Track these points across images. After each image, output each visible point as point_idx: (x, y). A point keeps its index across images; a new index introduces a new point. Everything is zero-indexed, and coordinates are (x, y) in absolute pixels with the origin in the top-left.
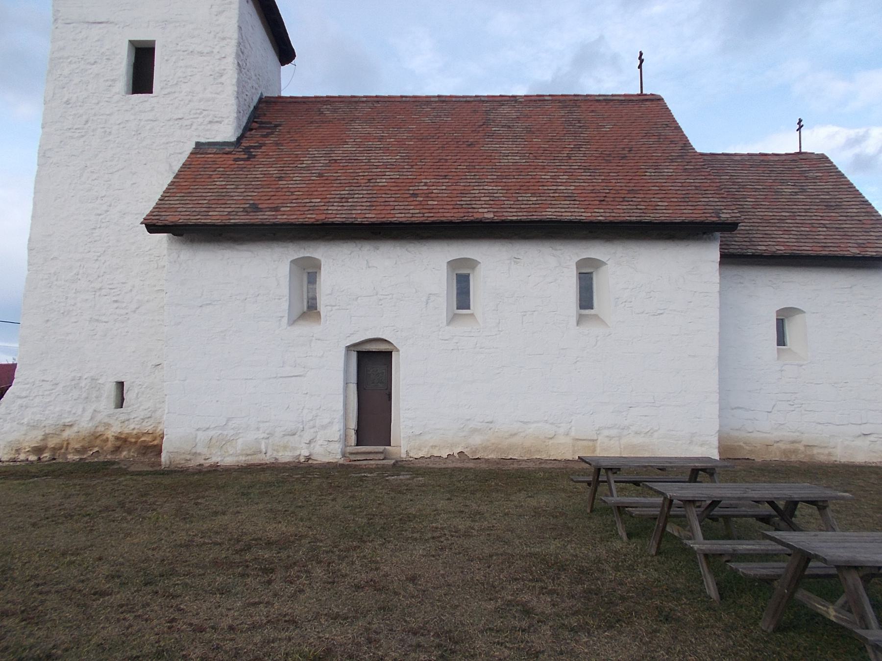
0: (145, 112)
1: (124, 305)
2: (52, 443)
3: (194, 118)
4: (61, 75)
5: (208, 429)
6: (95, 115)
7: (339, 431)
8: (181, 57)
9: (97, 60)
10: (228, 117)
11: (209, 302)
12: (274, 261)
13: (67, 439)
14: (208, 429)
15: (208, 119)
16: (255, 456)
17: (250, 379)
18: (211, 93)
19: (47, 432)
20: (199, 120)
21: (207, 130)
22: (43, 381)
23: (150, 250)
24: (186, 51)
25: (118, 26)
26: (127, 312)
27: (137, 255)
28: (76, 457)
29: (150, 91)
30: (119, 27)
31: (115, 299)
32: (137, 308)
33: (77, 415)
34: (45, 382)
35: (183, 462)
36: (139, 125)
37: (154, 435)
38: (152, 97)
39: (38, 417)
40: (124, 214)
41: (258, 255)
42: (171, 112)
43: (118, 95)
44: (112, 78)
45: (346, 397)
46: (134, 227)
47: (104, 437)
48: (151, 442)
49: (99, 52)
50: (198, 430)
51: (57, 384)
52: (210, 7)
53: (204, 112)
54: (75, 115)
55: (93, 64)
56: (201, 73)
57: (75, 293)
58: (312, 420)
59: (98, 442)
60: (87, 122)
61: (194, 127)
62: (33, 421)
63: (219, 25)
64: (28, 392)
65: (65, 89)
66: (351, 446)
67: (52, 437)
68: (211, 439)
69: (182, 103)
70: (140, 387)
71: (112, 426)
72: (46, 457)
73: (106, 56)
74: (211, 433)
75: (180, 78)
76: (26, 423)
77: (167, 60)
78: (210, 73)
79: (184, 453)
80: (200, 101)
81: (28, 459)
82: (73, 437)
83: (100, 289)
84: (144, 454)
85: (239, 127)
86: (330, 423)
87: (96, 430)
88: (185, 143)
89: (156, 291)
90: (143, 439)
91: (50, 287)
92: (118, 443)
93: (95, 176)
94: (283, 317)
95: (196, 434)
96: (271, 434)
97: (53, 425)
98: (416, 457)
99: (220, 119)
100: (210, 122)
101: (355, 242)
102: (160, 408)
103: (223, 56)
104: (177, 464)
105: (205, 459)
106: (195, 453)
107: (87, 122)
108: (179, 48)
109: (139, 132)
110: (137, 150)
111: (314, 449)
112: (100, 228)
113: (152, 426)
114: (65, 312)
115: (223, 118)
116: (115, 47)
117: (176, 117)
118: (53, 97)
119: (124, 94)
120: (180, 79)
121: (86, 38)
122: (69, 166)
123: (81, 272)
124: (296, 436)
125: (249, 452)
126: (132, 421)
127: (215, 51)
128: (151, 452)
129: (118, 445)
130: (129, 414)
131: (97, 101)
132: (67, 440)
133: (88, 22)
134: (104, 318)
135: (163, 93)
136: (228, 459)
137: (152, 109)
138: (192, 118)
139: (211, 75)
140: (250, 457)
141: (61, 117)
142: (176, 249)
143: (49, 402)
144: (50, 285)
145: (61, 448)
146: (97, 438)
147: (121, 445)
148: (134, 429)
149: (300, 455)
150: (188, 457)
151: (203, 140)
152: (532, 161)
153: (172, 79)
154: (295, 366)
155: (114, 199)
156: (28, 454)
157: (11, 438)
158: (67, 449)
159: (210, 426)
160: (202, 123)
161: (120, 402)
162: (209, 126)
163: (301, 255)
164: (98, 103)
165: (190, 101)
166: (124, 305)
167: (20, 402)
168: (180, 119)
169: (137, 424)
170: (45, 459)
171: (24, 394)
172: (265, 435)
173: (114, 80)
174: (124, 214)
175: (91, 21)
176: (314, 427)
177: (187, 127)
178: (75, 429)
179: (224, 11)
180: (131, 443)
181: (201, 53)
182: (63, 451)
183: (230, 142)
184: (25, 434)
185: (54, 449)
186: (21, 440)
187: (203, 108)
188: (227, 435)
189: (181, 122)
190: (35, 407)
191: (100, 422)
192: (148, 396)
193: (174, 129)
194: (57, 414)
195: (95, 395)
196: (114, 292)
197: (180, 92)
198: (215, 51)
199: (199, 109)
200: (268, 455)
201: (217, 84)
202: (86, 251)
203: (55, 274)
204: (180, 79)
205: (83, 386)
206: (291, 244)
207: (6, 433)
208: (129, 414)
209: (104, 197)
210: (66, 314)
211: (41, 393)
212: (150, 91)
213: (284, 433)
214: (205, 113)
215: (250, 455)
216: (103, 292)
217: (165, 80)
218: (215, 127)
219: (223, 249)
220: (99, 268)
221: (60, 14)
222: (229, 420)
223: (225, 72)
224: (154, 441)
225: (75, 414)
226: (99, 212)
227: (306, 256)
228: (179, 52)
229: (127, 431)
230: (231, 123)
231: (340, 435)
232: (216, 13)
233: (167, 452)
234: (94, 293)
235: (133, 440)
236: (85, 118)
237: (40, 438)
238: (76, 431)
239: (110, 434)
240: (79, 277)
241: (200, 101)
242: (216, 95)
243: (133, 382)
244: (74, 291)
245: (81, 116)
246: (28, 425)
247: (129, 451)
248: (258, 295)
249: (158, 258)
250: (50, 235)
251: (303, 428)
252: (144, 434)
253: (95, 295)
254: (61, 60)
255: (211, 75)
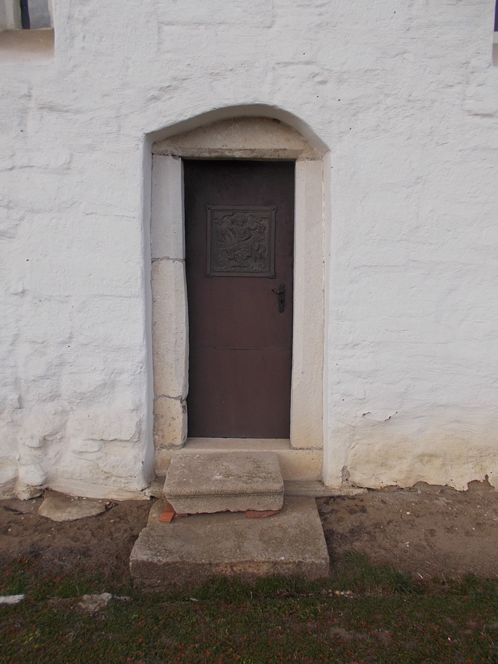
7: (136, 409)
45: (154, 301)
58: (44, 377)
66: (172, 446)
85: (185, 409)
86: (105, 385)
98: (371, 484)
111: (57, 462)
149: (15, 480)
176: (55, 396)
231: (139, 424)
251: (20, 399)
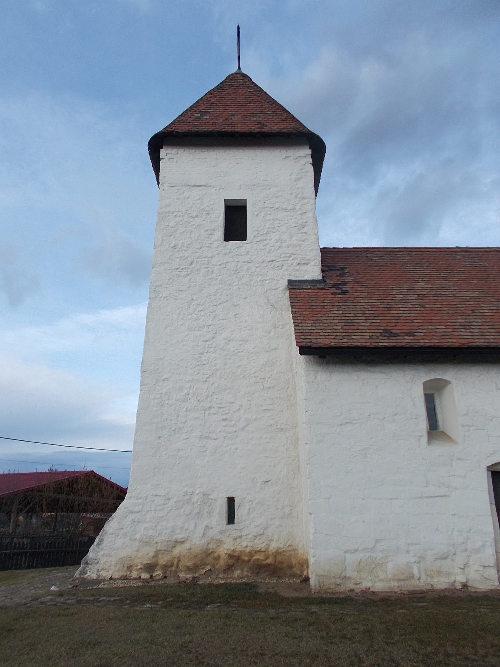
0: (241, 255)
1: (233, 423)
2: (163, 560)
3: (284, 261)
4: (168, 225)
5: (356, 551)
6: (198, 257)
8: (269, 213)
9: (199, 214)
10: (314, 260)
11: (349, 421)
12: (408, 382)
13: (178, 555)
14: (356, 551)
15: (297, 261)
16: (407, 582)
17: (395, 499)
18: (297, 240)
19: (159, 548)
20: (288, 262)
21: (297, 270)
22: (156, 495)
23: (255, 372)
24: (272, 208)
25: (215, 189)
26: (235, 429)
27: (243, 377)
28: (188, 576)
29: (245, 239)
30: (216, 189)
31: (224, 417)
32: (245, 426)
33: (188, 531)
34: (157, 497)
35: (333, 586)
36: (237, 266)
37: (267, 553)
38: (246, 243)
39: (150, 533)
40: (229, 341)
41: (391, 376)
42: (264, 255)
43: (217, 242)
44: (212, 228)
46: (238, 352)
47: (216, 555)
48: (264, 560)
49: (199, 208)
50: (346, 552)
51: (170, 499)
52: (290, 175)
53: (292, 255)
54: (181, 257)
55: (195, 218)
56: (287, 225)
57: (186, 411)
58: (463, 543)
59: (209, 559)
60: (192, 263)
61: (285, 268)
62: (145, 537)
63: (298, 188)
64: (140, 507)
65: (172, 237)
67: (163, 554)
68: (360, 562)
69: (273, 248)
70: (251, 503)
71: (225, 543)
72: (159, 575)
73: (206, 211)
74: (360, 556)
75: (269, 228)
76: (138, 539)
77: (257, 215)
78: (294, 225)
79: (334, 577)
80: (288, 246)
81: (140, 577)
82: (184, 553)
83: (210, 408)
84: (258, 573)
87: (208, 548)
88: (279, 280)
89: (263, 410)
90: (255, 557)
91: (162, 405)
92: (231, 561)
93: (201, 308)
94: (421, 436)
95: (345, 557)
96: (422, 558)
97: (165, 541)
99: (307, 262)
100: (299, 264)
101: (408, 366)
102: (271, 525)
103: (304, 211)
104: (327, 589)
105: (356, 584)
106: (345, 577)
107: (192, 263)
108: (266, 205)
109: (238, 272)
110: (237, 287)
112: (207, 352)
113: (265, 544)
114: (176, 429)
115: (310, 260)
116: (213, 204)
117: (268, 259)
118: (162, 243)
119: (222, 241)
120: (270, 230)
121: (189, 197)
122: (177, 299)
123: (191, 392)
124: (448, 560)
125: (402, 577)
126: (244, 538)
127: (298, 207)
128: (265, 572)
129: (232, 564)
130: (241, 530)
131: (200, 247)
132: (179, 557)
133: (189, 186)
134: (214, 436)
135: (256, 240)
136: (378, 584)
137: (248, 253)
138: (282, 261)
139: (296, 226)
140: (402, 583)
141: (169, 259)
142: (313, 371)
143: (162, 517)
144: (161, 404)
145: (172, 566)
146: (208, 555)
147: (234, 564)
148: (247, 546)
149: (455, 581)
150: (338, 581)
151: (294, 278)
152: (320, 310)
153: (262, 229)
154: (439, 486)
155: (219, 328)
156: (140, 571)
157: (123, 554)
158: (177, 566)
159: (358, 548)
160: (292, 264)
161: (231, 519)
162: (298, 267)
163: (433, 378)
164: (200, 248)
165: (279, 247)
166: (233, 423)
167: (132, 517)
168: (272, 261)
169: (250, 542)
170: (158, 578)
171: (137, 509)
172: (417, 559)
173: (213, 230)
174: (229, 341)
175: (192, 185)
176: (466, 550)
177: (278, 268)
178: (187, 545)
179: (302, 178)
180: (244, 561)
181: (285, 210)
182: (174, 568)
183: (317, 280)
184: (137, 551)
185: (165, 568)
186: (133, 556)
187: (291, 252)
188: (376, 558)
189: (273, 264)
190: (148, 522)
191: (212, 539)
192: (260, 512)
193: (267, 269)
194: (170, 530)
195: (206, 510)
196: (223, 411)
197: (271, 240)
198: (298, 207)
199: (288, 253)
200: (421, 581)
201: (301, 233)
202: (195, 373)
203: (166, 393)
204: (270, 230)
205: (195, 501)
206: (421, 367)
207: (117, 549)
208: (241, 530)
209: (210, 325)
210: (177, 431)
211: (153, 508)
212: (245, 239)
213: (435, 557)
214: (293, 256)
215: (403, 580)
216: (213, 411)
217: (257, 230)
218: (304, 268)
219: (357, 371)
220: (207, 389)
221: (166, 179)
222: (377, 541)
223: (307, 224)
224: (266, 559)
225: (187, 530)
226: (206, 339)
227: (437, 378)
228: (267, 209)
229: (239, 548)
230: (317, 264)
232: (295, 180)
233: (317, 575)
234: (204, 412)
235: (246, 558)
236: (190, 260)
237: (152, 554)
238: (188, 548)
239: (223, 550)
240: (190, 396)
241: (288, 246)
242: (301, 242)
243: (244, 498)
244: (185, 409)
245: (187, 258)
246: (140, 540)
247: (242, 570)
248: (396, 414)
249: (264, 380)
250: (161, 359)
252: (256, 552)
253: (204, 413)
254: (168, 214)
255: (296, 226)
